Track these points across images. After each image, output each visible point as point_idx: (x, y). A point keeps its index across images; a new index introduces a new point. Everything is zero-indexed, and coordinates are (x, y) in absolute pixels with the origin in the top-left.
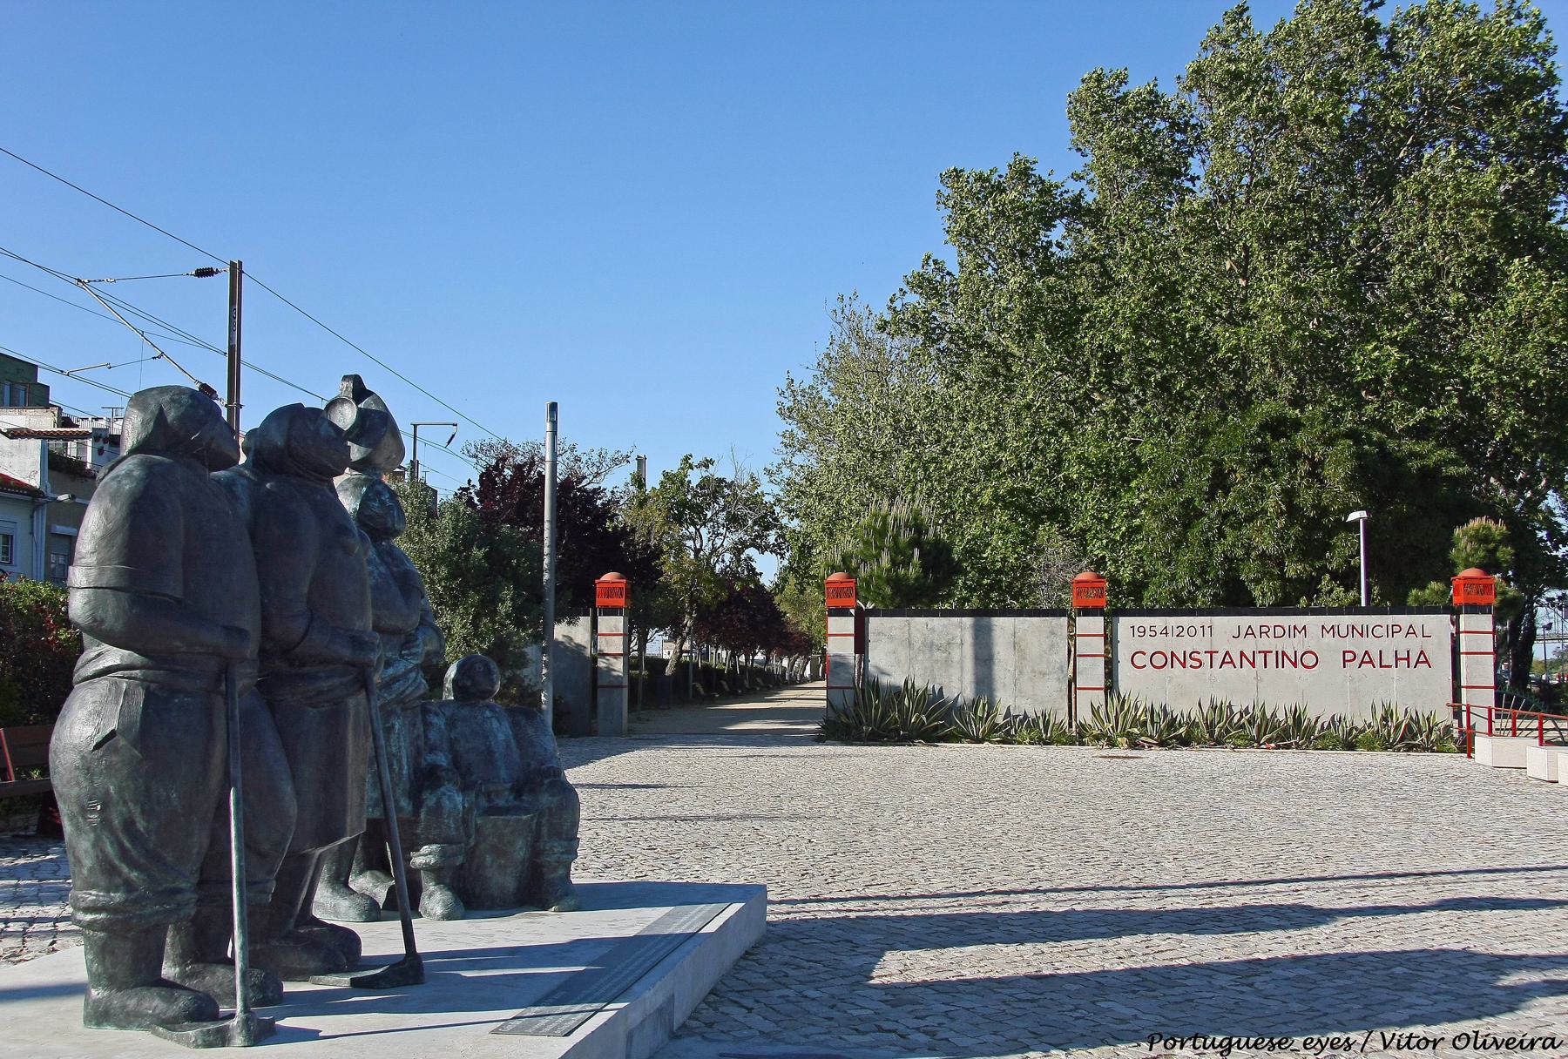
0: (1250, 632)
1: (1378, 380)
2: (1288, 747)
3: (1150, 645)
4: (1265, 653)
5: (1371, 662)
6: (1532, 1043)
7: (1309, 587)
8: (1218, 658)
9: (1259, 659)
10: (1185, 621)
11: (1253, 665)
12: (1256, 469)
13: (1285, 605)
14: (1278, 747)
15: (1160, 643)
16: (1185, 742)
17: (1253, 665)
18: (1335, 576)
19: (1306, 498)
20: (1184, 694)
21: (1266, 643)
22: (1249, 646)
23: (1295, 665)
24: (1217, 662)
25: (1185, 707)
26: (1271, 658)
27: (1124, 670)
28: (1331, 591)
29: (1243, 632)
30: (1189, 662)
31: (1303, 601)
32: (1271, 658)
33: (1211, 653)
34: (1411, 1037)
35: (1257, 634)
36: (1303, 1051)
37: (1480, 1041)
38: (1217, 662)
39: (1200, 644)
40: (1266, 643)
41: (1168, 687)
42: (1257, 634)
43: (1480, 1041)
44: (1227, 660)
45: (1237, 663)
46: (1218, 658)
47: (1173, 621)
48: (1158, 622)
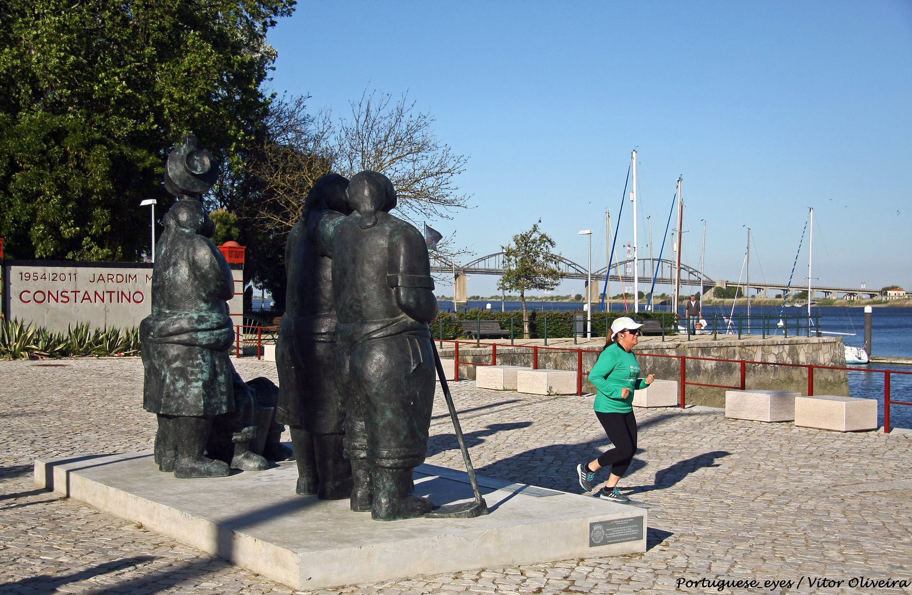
0: (101, 278)
1: (106, 100)
2: (129, 355)
3: (33, 286)
4: (111, 292)
5: (89, 299)
6: (894, 584)
7: (75, 243)
8: (80, 296)
9: (107, 296)
10: (58, 270)
11: (103, 300)
12: (40, 164)
13: (57, 259)
14: (126, 355)
15: (40, 285)
16: (64, 354)
17: (103, 300)
18: (93, 238)
19: (76, 183)
20: (58, 321)
21: (111, 286)
22: (100, 287)
23: (129, 300)
24: (79, 299)
25: (59, 330)
26: (114, 296)
27: (15, 303)
28: (91, 248)
29: (97, 278)
30: (60, 298)
31: (70, 256)
32: (114, 296)
33: (76, 292)
34: (825, 580)
35: (106, 279)
36: (764, 588)
37: (864, 582)
38: (79, 299)
39: (68, 286)
40: (100, 287)
41: (46, 316)
42: (106, 279)
43: (864, 582)
44: (86, 297)
45: (93, 300)
46: (80, 296)
47: (50, 270)
48: (39, 270)
